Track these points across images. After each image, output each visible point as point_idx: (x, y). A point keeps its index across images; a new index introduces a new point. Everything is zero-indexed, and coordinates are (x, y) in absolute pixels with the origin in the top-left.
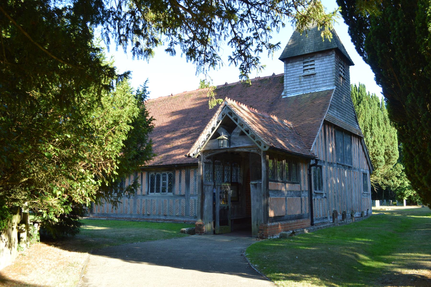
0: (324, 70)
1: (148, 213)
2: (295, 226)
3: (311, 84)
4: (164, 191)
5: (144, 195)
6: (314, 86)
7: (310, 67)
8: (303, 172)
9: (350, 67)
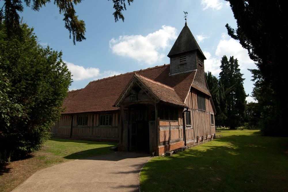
0: (191, 61)
1: (99, 136)
2: (176, 146)
3: (184, 68)
4: (107, 124)
5: (97, 126)
7: (183, 60)
9: (204, 60)
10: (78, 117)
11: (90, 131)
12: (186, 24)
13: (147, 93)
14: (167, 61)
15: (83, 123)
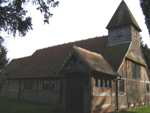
0: (127, 34)
1: (42, 99)
13: (83, 63)
14: (106, 33)
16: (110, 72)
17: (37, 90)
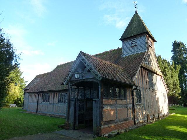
4: (47, 102)
6: (136, 51)
8: (128, 93)
10: (43, 95)
11: (51, 107)
12: (136, 11)
14: (119, 45)
15: (47, 101)
16: (125, 79)
17: (54, 103)
